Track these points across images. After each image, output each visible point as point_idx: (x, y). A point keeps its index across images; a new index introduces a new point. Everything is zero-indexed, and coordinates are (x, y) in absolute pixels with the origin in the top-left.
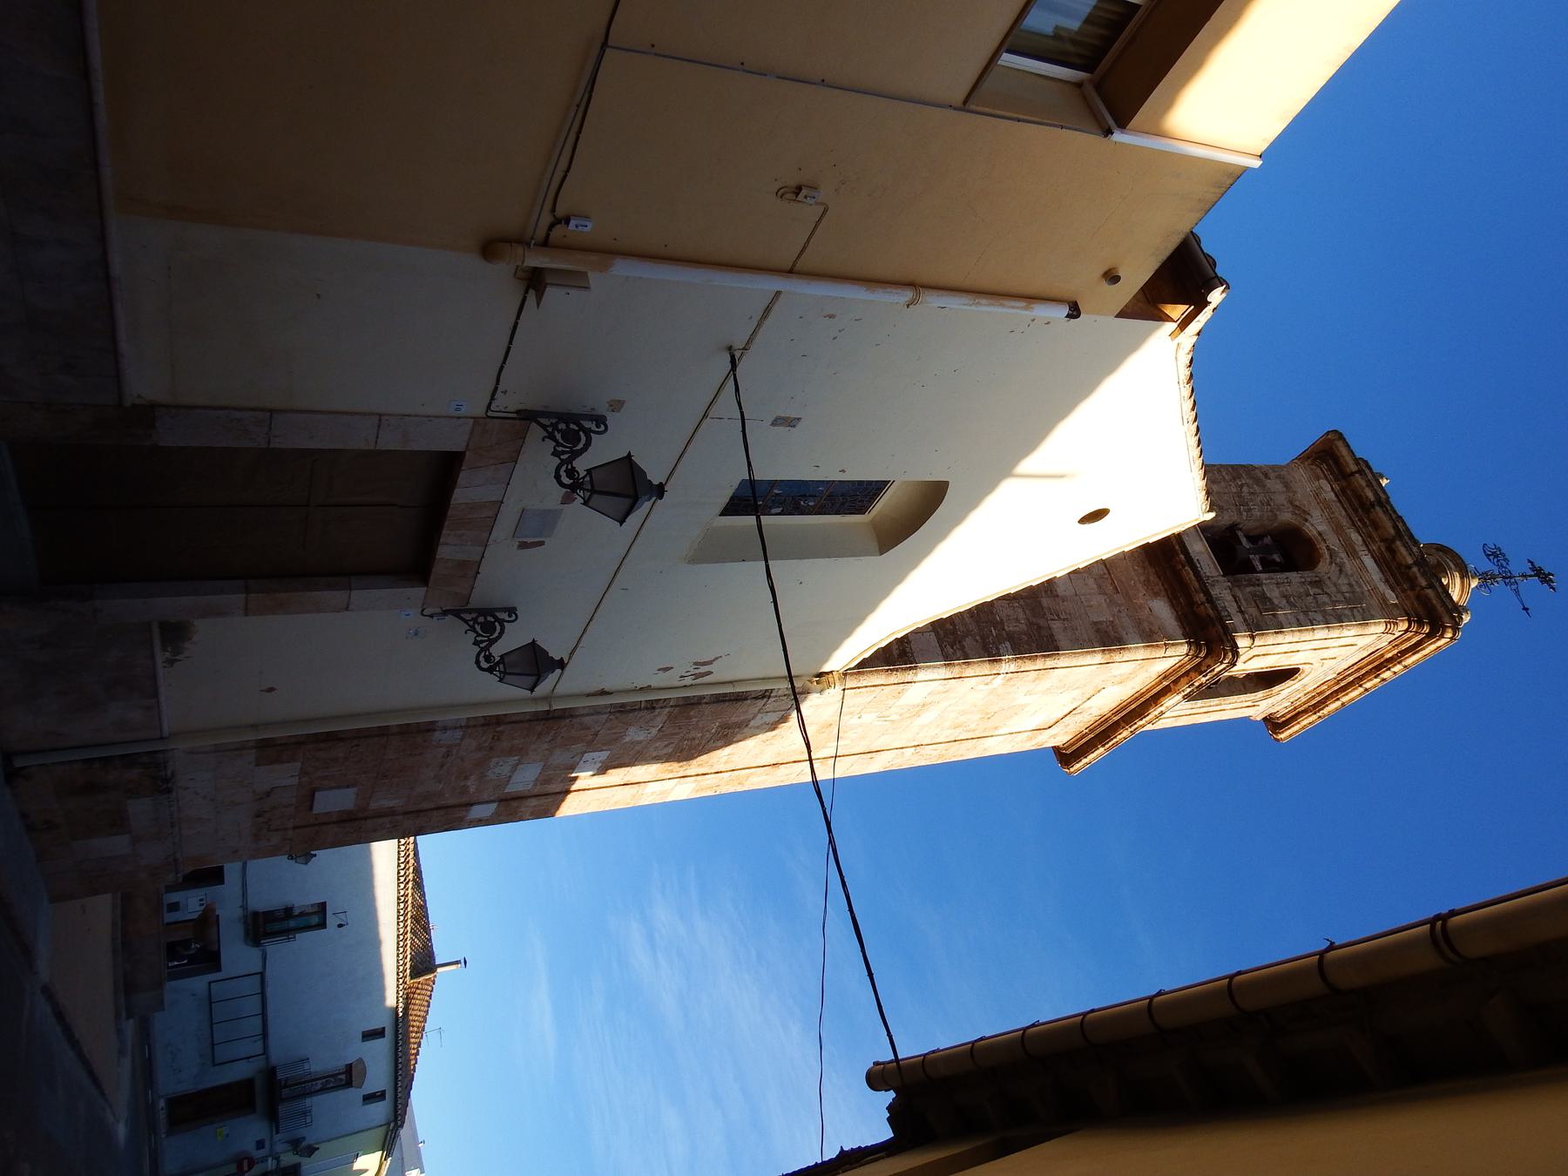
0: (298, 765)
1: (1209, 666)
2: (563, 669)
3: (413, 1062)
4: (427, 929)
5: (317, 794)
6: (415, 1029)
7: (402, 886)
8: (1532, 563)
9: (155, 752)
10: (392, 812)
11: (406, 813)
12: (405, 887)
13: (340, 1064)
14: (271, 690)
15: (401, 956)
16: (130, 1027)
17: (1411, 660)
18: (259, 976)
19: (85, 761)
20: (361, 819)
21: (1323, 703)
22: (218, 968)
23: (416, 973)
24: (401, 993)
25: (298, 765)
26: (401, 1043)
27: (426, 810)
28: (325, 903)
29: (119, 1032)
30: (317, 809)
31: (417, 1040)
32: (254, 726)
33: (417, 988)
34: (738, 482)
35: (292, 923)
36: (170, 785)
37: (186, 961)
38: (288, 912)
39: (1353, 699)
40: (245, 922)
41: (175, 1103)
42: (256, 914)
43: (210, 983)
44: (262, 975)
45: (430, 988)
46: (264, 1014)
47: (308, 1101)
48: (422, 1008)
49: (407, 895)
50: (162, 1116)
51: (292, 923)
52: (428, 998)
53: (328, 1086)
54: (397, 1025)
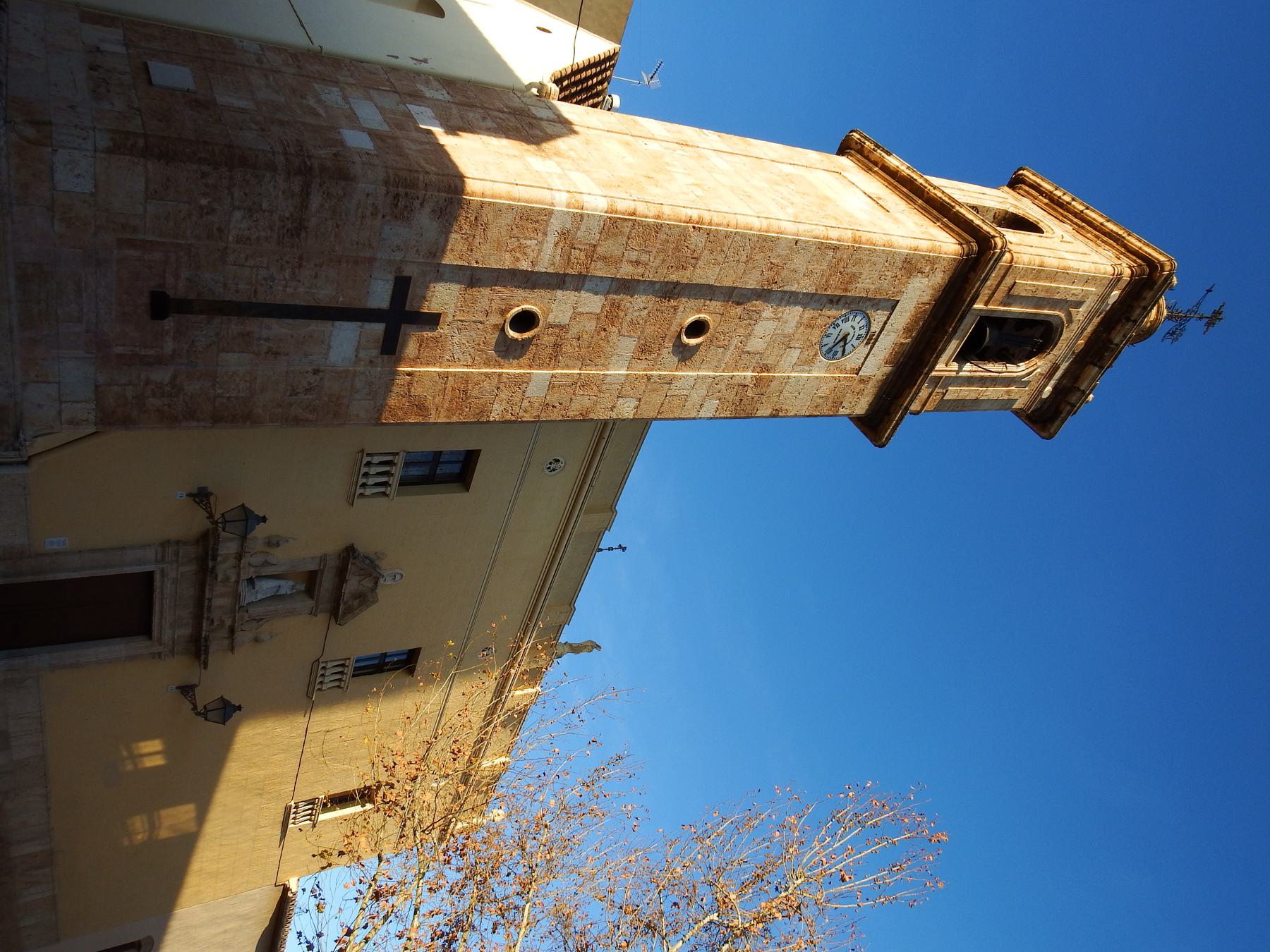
1: (857, 143)
8: (1205, 332)
17: (1047, 186)
21: (1110, 235)
34: (253, 510)
39: (1154, 249)
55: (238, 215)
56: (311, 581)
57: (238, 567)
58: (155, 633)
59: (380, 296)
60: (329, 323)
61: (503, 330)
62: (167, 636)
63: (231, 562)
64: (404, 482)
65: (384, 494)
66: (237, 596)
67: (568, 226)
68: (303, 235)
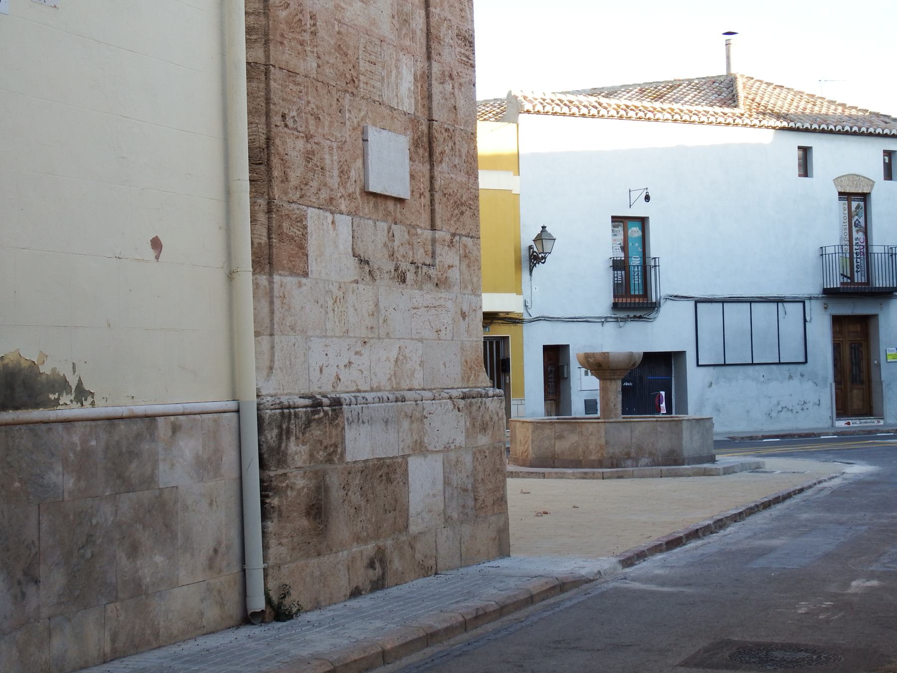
0: (311, 212)
2: (824, 289)
3: (854, 112)
4: (673, 86)
5: (371, 189)
6: (810, 106)
7: (603, 112)
9: (260, 419)
10: (425, 79)
11: (429, 58)
12: (606, 108)
13: (838, 208)
14: (156, 244)
15: (704, 119)
16: (725, 459)
18: (699, 305)
19: (265, 516)
20: (430, 127)
22: (680, 355)
23: (732, 100)
24: (756, 122)
25: (311, 212)
26: (824, 126)
27: (428, 24)
28: (613, 217)
29: (728, 471)
30: (402, 189)
31: (826, 104)
32: (231, 275)
33: (753, 100)
35: (635, 261)
36: (325, 401)
37: (663, 393)
38: (618, 265)
40: (624, 320)
41: (843, 409)
42: (615, 307)
43: (698, 365)
44: (698, 301)
45: (758, 84)
46: (751, 301)
47: (876, 249)
48: (782, 95)
49: (627, 107)
50: (856, 423)
51: (635, 261)
52: (771, 87)
53: (863, 224)
54: (798, 130)
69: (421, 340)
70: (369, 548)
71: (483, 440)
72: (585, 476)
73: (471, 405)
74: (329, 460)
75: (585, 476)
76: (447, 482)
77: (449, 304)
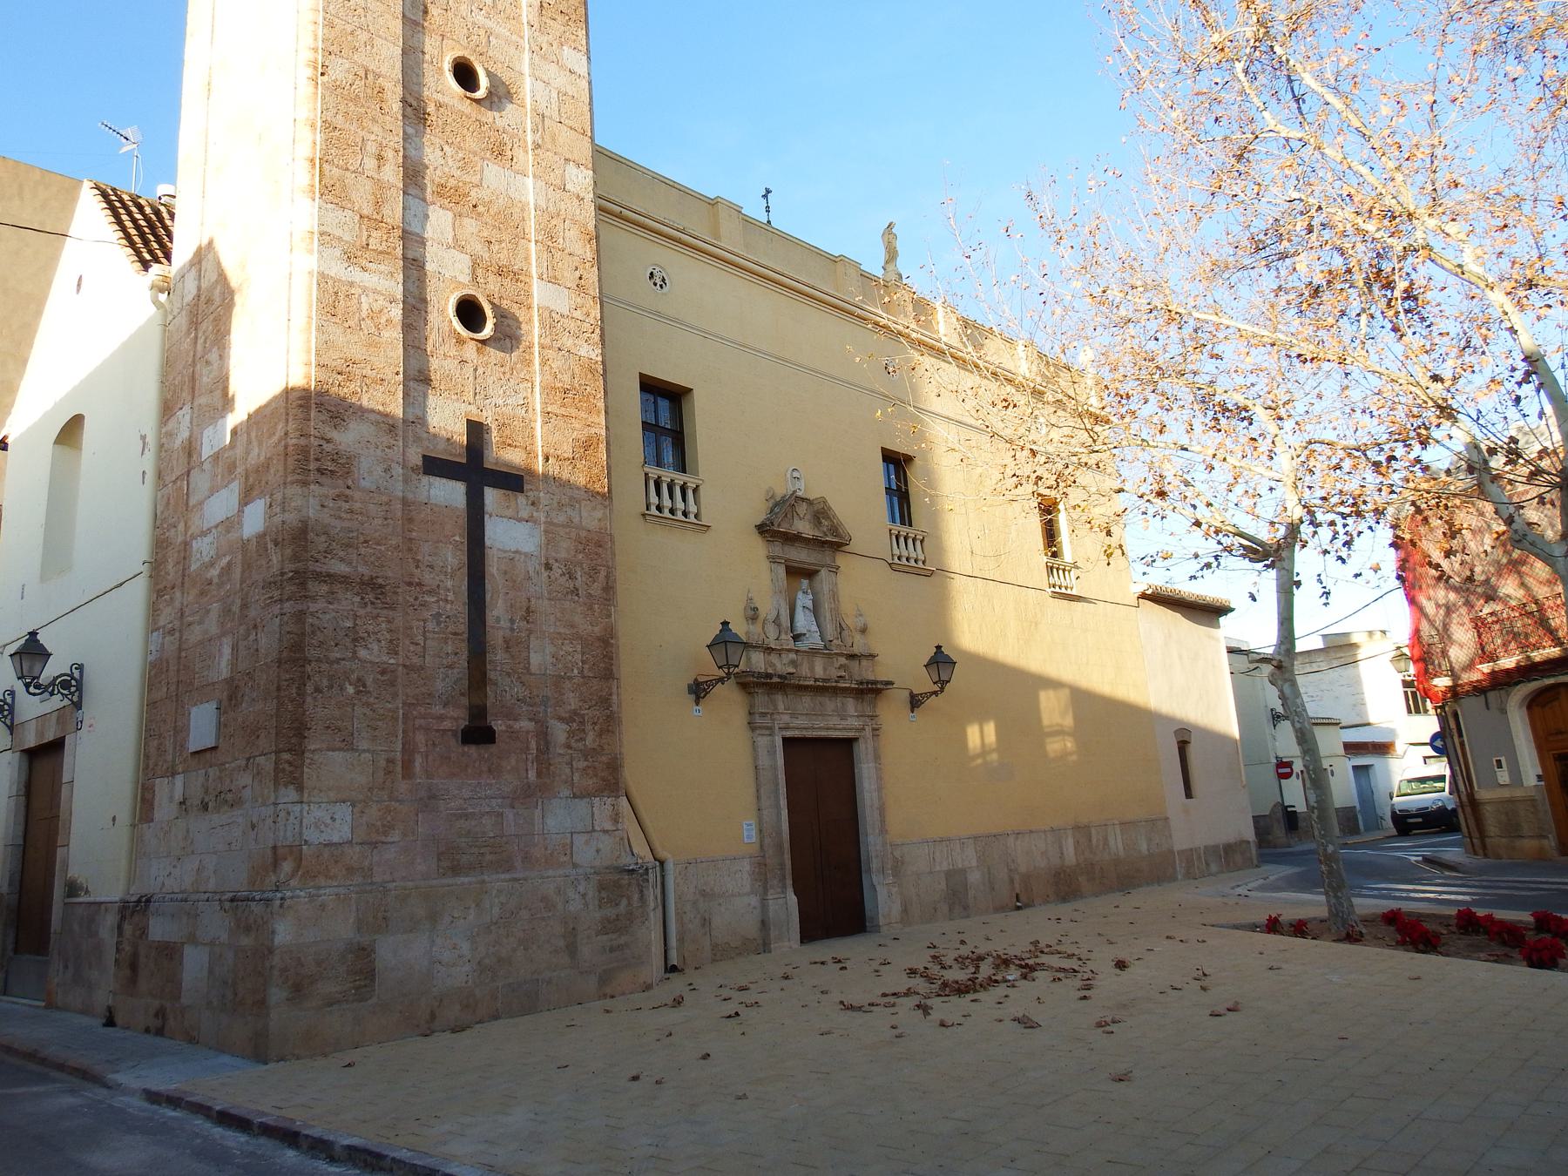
55: (362, 653)
56: (796, 572)
57: (779, 652)
58: (851, 734)
59: (452, 493)
60: (487, 551)
61: (483, 342)
62: (856, 723)
63: (774, 658)
64: (682, 467)
65: (695, 490)
66: (813, 652)
67: (338, 252)
68: (380, 581)
69: (215, 853)
70: (156, 1003)
71: (246, 941)
72: (1065, 399)
73: (237, 907)
74: (141, 937)
75: (1065, 399)
76: (211, 972)
77: (240, 820)
